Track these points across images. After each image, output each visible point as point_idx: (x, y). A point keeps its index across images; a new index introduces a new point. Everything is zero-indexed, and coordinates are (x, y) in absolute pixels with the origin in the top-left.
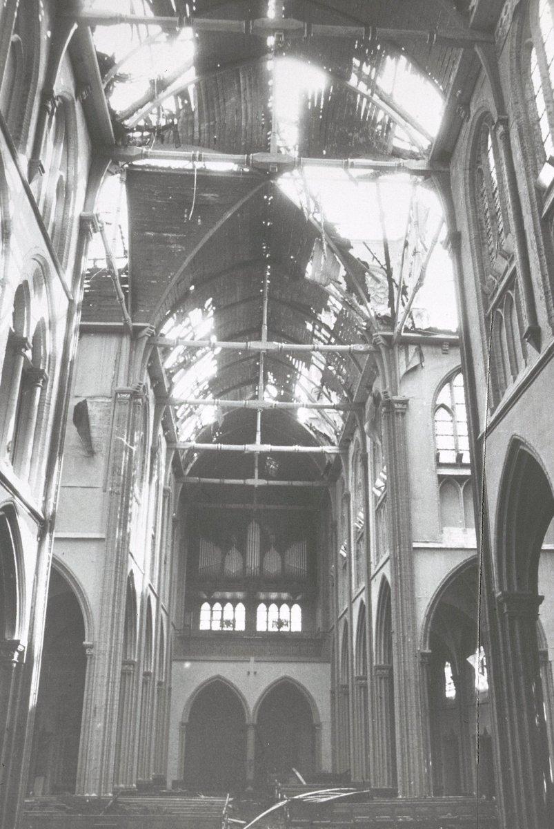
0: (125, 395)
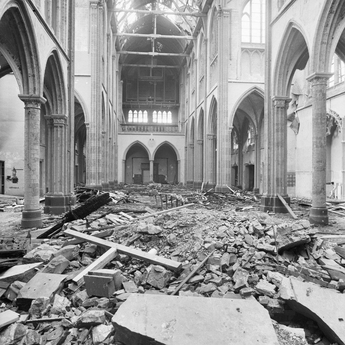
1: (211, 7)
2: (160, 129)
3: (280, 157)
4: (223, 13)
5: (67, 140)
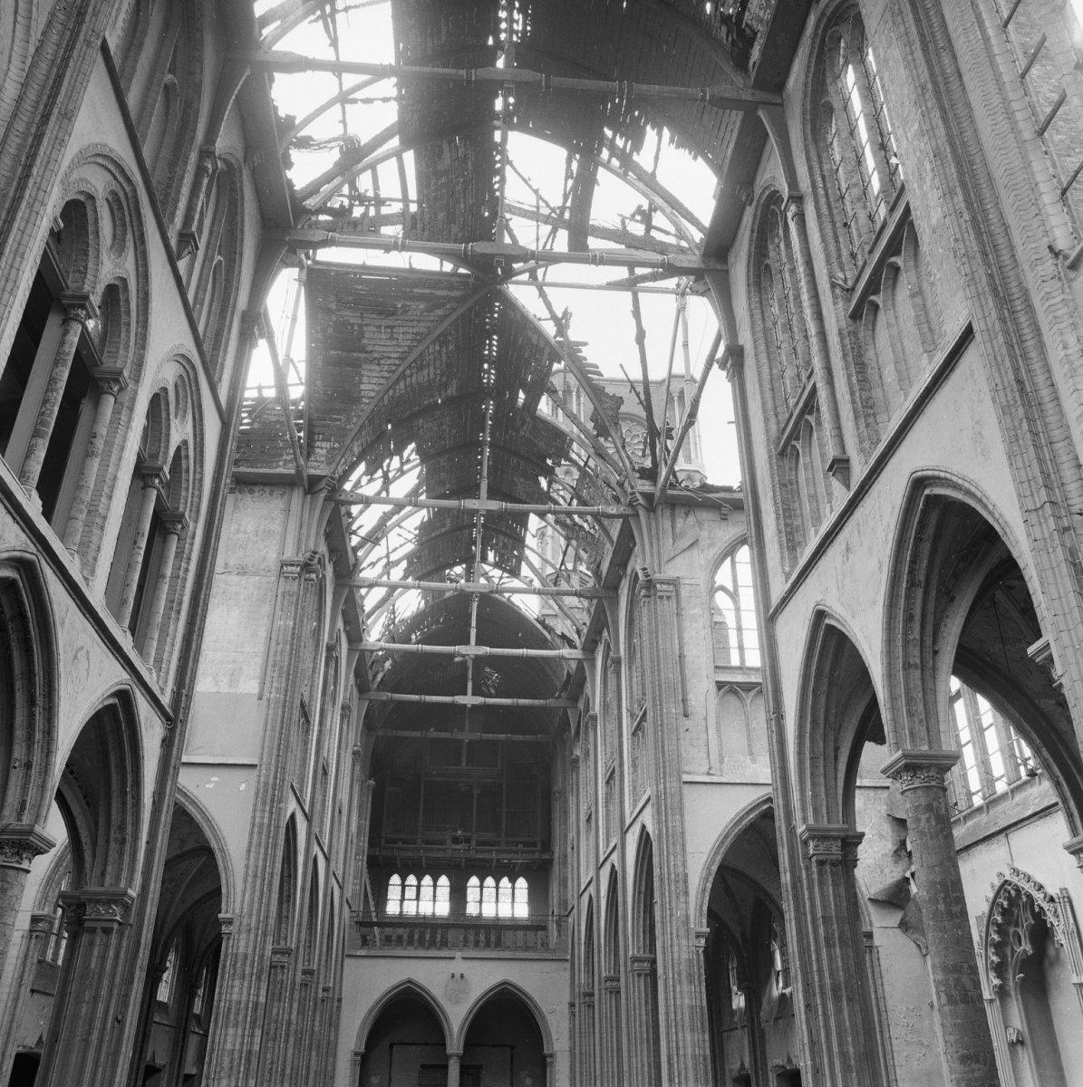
0: (294, 568)
1: (625, 573)
2: (492, 935)
3: (850, 1039)
4: (655, 587)
5: (118, 980)
